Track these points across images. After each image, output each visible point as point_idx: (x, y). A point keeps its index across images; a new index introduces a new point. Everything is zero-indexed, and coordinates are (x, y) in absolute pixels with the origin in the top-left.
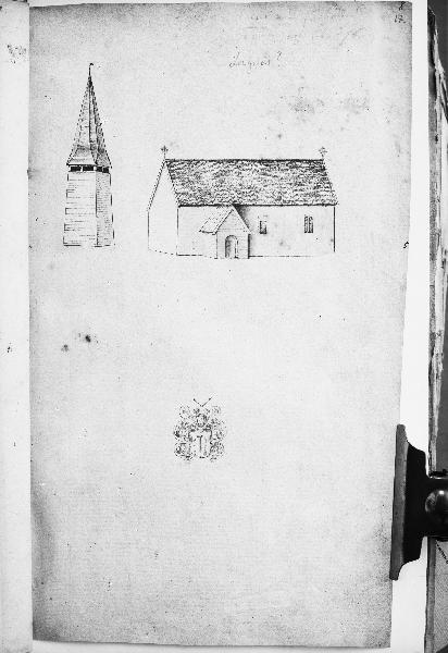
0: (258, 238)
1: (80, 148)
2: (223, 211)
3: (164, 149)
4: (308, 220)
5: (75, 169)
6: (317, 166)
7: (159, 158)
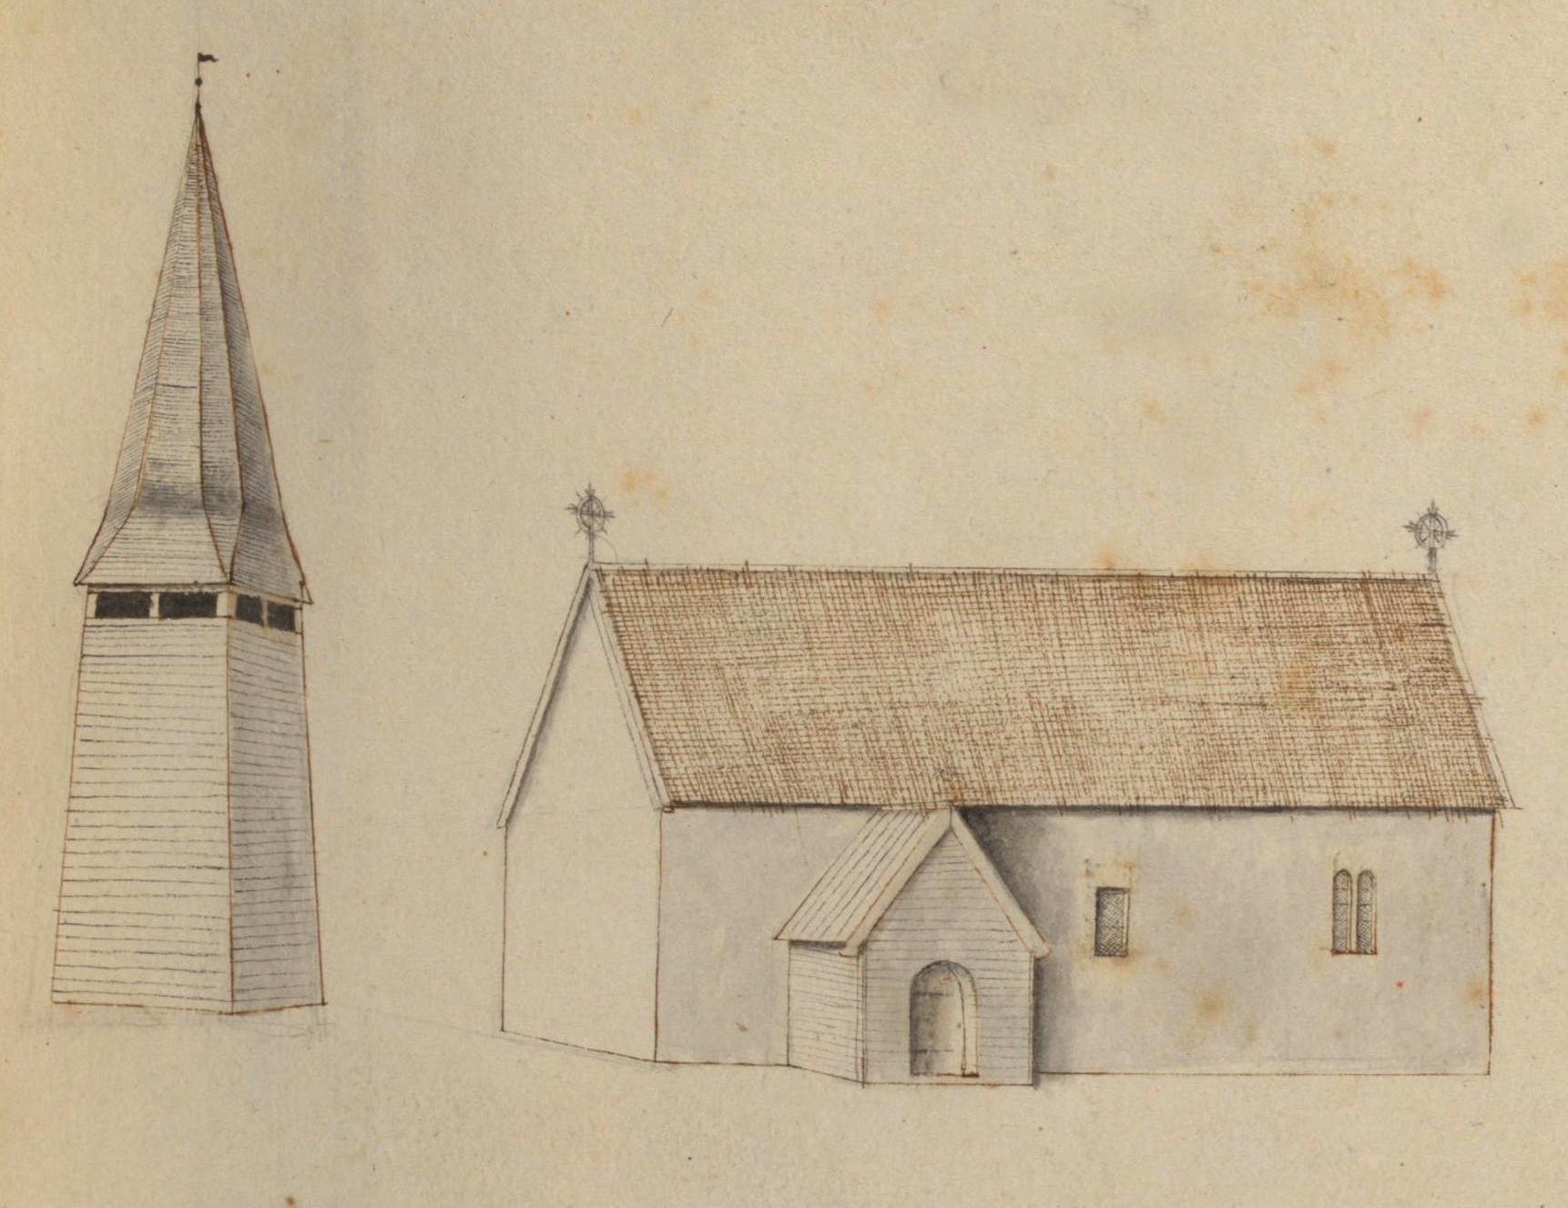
0: (1091, 980)
1: (156, 500)
2: (905, 838)
3: (590, 511)
4: (1352, 886)
5: (119, 604)
6: (1101, 892)
7: (567, 554)
